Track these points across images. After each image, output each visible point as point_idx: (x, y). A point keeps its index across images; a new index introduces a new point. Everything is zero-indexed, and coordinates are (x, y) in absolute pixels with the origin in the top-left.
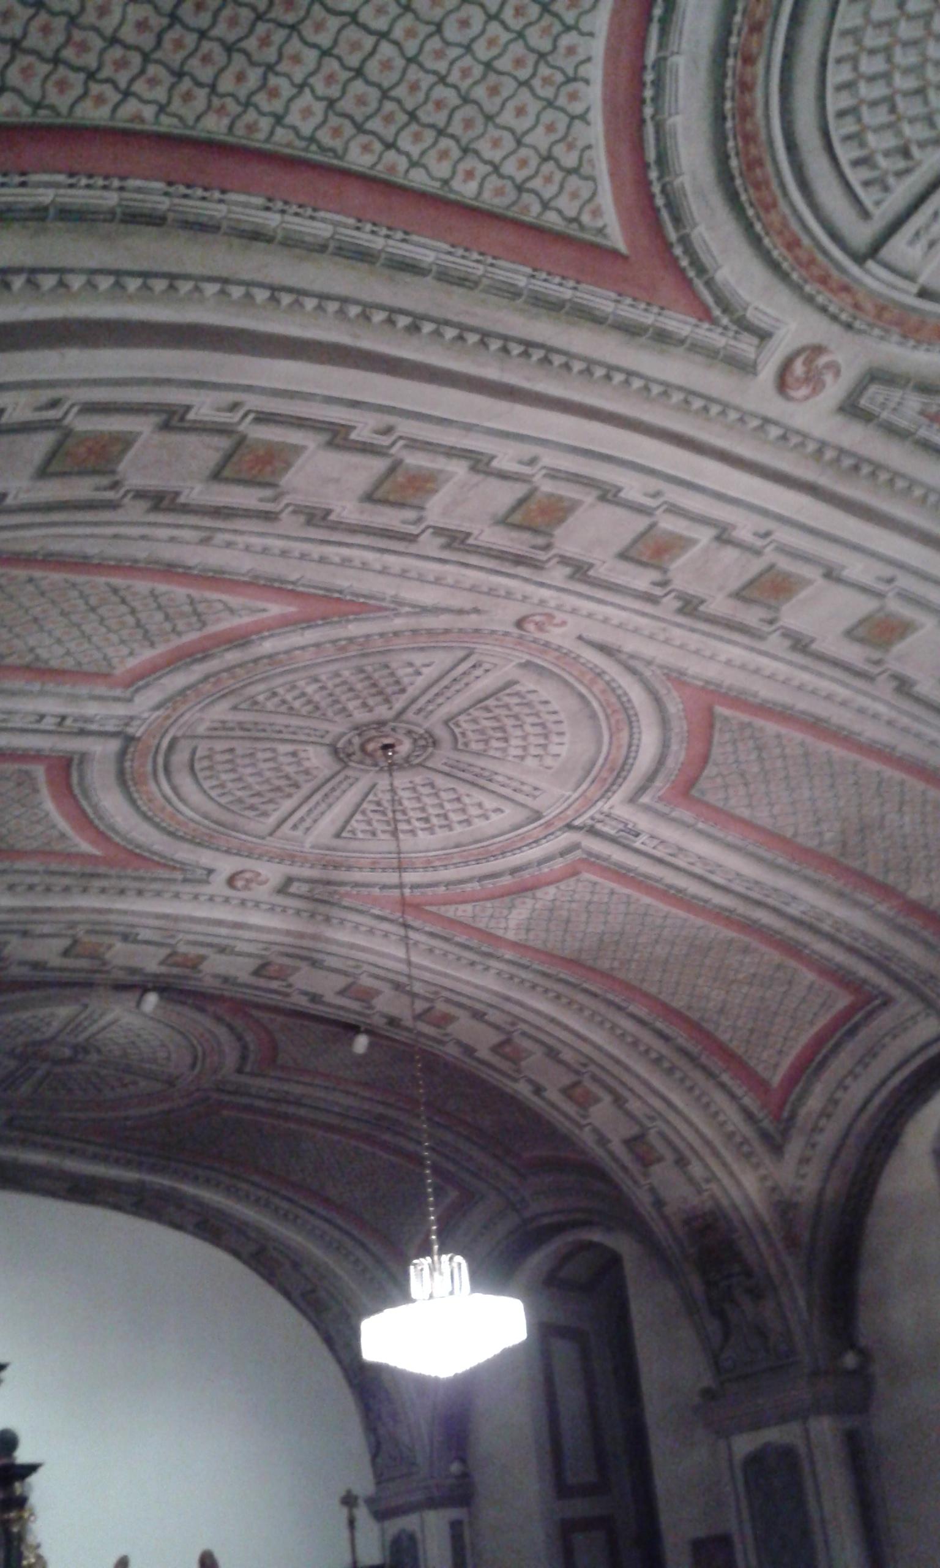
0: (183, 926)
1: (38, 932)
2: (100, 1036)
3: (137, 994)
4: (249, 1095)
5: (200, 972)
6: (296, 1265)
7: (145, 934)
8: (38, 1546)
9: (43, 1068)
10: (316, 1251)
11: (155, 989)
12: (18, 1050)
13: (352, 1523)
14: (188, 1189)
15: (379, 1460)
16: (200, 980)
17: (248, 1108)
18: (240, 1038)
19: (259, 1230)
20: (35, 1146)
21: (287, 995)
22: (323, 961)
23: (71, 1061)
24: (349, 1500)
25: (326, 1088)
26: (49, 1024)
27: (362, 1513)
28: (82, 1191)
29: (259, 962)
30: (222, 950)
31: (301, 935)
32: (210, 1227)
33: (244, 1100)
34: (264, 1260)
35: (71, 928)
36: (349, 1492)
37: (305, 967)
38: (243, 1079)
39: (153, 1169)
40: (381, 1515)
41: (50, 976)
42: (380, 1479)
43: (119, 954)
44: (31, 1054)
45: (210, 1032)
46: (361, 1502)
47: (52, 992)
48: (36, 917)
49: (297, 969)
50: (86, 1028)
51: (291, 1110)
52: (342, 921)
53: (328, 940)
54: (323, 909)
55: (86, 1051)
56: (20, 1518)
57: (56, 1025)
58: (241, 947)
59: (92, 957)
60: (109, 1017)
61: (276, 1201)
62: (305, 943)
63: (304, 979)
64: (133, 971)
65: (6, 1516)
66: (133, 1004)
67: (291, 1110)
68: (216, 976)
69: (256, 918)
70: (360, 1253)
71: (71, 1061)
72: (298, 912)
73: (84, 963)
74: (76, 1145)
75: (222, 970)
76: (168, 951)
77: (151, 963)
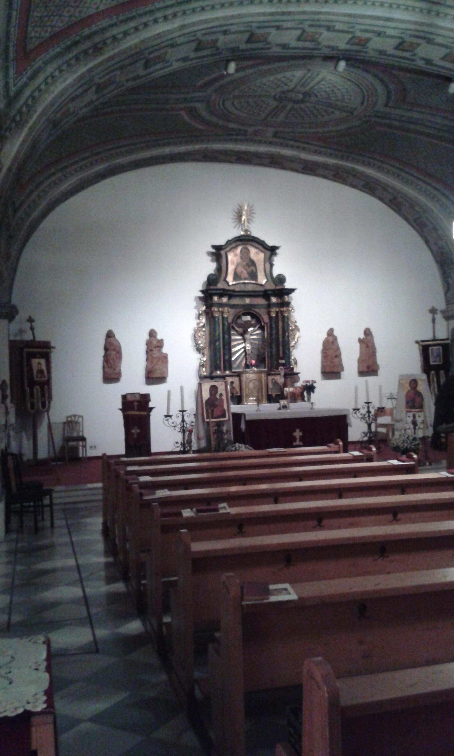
0: (360, 20)
1: (285, 26)
2: (316, 87)
3: (335, 62)
4: (389, 118)
5: (367, 48)
6: (412, 206)
7: (338, 26)
8: (296, 322)
9: (289, 106)
10: (422, 199)
11: (344, 58)
12: (277, 97)
13: (434, 321)
14: (360, 168)
15: (449, 295)
16: (366, 53)
17: (390, 126)
18: (386, 86)
19: (394, 189)
20: (287, 146)
21: (414, 60)
22: (433, 39)
23: (302, 101)
24: (433, 311)
25: (432, 114)
26: (291, 81)
27: (439, 317)
28: (309, 169)
29: (400, 41)
30: (379, 34)
31: (422, 24)
32: (369, 187)
33: (387, 121)
34: (395, 202)
35: (301, 23)
36: (433, 308)
37: (424, 44)
38: (388, 110)
39: (342, 158)
40: (447, 318)
41: (290, 52)
42: (448, 302)
43: (327, 39)
44: (283, 98)
45: (371, 83)
46: (439, 312)
47: (292, 62)
48: (284, 18)
49: (419, 45)
50: (309, 83)
51: (412, 127)
52: (446, 15)
53: (437, 27)
54: (435, 8)
55: (310, 96)
56: (288, 310)
57: (295, 81)
58: (390, 32)
59: (313, 41)
60: (320, 77)
61: (403, 174)
62: (426, 29)
63: (424, 51)
64: (333, 48)
65: (282, 309)
66: (333, 68)
67: (412, 127)
68: (375, 50)
69: (398, 15)
70: (444, 200)
71: (302, 101)
72: (421, 10)
73: (308, 45)
74: (306, 146)
75: (379, 47)
76: (350, 36)
77: (341, 43)
